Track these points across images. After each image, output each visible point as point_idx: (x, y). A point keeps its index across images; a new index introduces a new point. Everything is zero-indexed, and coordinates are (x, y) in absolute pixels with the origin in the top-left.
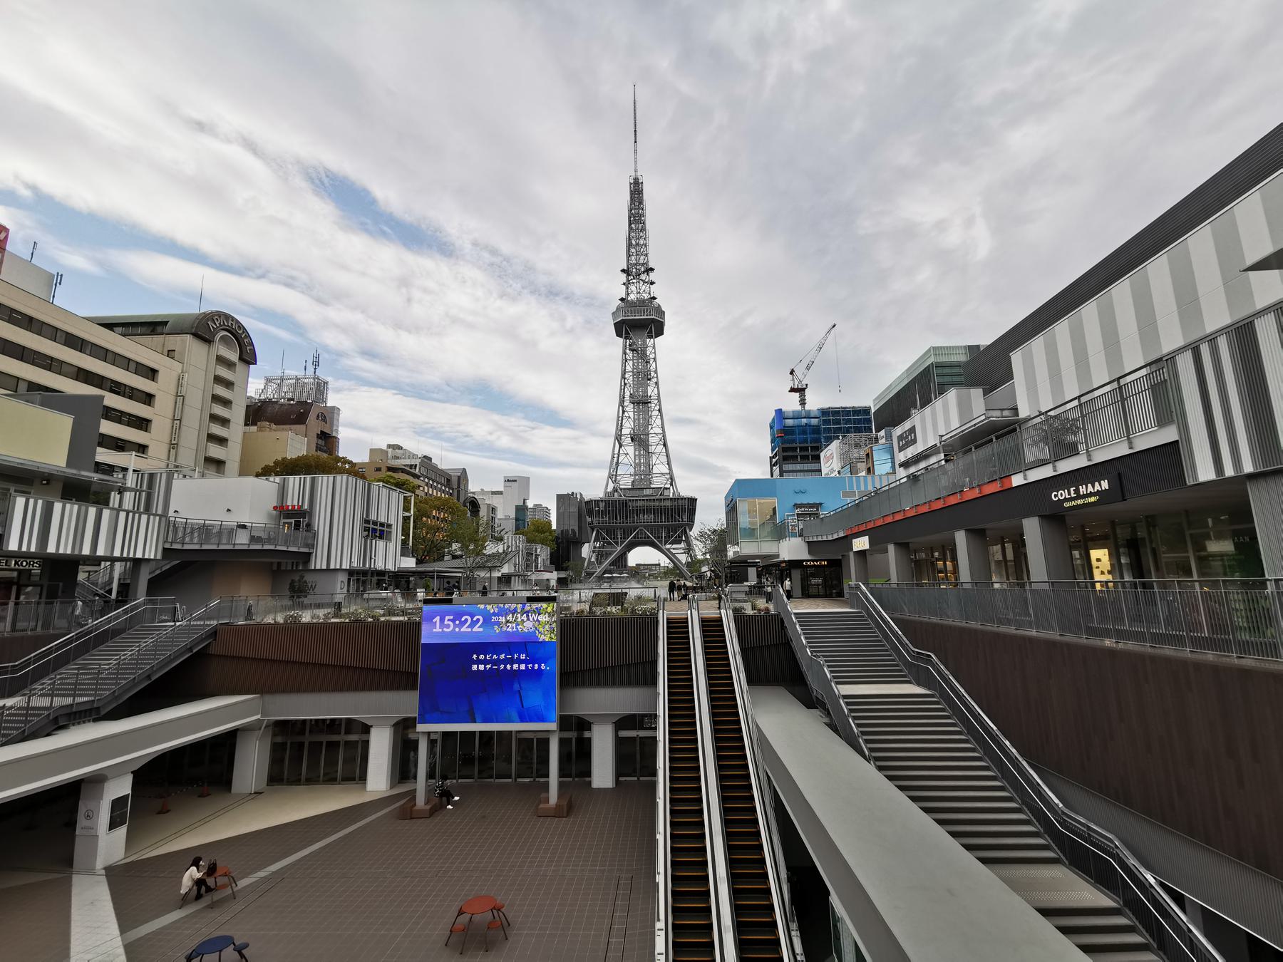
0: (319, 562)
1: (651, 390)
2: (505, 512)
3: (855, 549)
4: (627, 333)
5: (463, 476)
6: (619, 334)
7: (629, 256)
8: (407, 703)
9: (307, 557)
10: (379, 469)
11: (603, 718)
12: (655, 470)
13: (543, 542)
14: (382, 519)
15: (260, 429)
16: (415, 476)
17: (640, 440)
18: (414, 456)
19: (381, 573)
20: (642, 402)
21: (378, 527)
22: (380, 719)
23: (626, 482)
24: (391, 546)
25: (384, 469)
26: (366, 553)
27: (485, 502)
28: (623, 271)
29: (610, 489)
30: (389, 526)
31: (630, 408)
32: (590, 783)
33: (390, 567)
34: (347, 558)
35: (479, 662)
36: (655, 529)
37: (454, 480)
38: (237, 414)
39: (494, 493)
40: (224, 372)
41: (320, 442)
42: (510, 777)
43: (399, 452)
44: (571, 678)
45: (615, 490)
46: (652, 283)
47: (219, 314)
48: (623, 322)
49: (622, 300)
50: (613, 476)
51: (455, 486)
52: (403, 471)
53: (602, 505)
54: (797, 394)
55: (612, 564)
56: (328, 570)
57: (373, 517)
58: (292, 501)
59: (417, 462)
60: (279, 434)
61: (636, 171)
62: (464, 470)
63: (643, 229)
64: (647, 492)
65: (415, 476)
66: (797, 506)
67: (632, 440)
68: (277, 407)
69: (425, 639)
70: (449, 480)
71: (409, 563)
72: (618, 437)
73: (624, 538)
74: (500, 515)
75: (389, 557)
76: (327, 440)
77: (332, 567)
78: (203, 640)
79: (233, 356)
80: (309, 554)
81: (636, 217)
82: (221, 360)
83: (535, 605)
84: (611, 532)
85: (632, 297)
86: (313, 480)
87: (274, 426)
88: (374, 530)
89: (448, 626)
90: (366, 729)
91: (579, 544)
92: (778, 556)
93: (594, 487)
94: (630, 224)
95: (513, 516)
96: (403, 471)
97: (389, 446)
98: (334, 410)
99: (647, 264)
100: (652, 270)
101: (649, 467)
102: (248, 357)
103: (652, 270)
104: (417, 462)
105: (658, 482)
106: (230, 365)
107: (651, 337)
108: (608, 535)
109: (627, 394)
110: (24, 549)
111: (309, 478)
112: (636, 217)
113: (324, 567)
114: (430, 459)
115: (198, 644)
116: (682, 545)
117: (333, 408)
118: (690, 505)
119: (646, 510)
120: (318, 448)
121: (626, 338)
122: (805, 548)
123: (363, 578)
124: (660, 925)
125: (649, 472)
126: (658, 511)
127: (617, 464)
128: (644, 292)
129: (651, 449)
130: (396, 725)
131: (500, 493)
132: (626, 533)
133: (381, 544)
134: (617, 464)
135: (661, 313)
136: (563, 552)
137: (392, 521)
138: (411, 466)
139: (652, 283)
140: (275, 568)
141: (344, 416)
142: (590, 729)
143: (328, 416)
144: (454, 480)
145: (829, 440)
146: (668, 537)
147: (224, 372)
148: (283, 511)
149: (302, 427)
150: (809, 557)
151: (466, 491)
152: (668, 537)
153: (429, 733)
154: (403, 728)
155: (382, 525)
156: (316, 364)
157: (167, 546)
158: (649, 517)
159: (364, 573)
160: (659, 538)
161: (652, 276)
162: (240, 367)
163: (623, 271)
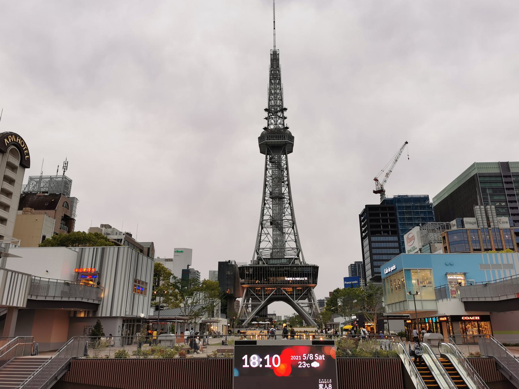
0: (104, 312)
1: (285, 190)
6: (262, 152)
12: (287, 246)
14: (143, 279)
15: (24, 213)
17: (276, 224)
20: (278, 198)
23: (266, 254)
24: (146, 298)
30: (147, 283)
31: (270, 203)
34: (121, 310)
37: (146, 250)
38: (14, 202)
39: (167, 260)
40: (10, 173)
41: (63, 222)
43: (109, 231)
45: (259, 259)
47: (12, 134)
50: (258, 250)
53: (251, 270)
54: (379, 195)
55: (257, 314)
57: (139, 278)
58: (86, 267)
59: (123, 237)
60: (37, 217)
61: (275, 46)
62: (153, 243)
63: (279, 83)
64: (283, 261)
68: (36, 197)
76: (68, 221)
77: (114, 315)
78: (61, 372)
79: (16, 162)
80: (98, 305)
81: (275, 75)
85: (272, 127)
86: (103, 249)
87: (33, 211)
93: (244, 258)
97: (102, 226)
98: (74, 200)
99: (282, 106)
100: (286, 109)
101: (283, 242)
102: (25, 163)
103: (286, 109)
104: (123, 237)
105: (290, 254)
106: (13, 168)
110: (8, 304)
112: (275, 75)
113: (108, 315)
114: (131, 235)
115: (59, 375)
116: (306, 301)
117: (74, 198)
118: (313, 272)
123: (132, 323)
125: (283, 248)
129: (286, 230)
133: (141, 297)
137: (148, 281)
138: (118, 240)
140: (72, 315)
143: (70, 204)
144: (146, 250)
145: (413, 225)
147: (10, 173)
148: (80, 275)
149: (52, 212)
150: (465, 313)
155: (143, 283)
156: (65, 168)
157: (29, 298)
161: (286, 114)
162: (19, 169)
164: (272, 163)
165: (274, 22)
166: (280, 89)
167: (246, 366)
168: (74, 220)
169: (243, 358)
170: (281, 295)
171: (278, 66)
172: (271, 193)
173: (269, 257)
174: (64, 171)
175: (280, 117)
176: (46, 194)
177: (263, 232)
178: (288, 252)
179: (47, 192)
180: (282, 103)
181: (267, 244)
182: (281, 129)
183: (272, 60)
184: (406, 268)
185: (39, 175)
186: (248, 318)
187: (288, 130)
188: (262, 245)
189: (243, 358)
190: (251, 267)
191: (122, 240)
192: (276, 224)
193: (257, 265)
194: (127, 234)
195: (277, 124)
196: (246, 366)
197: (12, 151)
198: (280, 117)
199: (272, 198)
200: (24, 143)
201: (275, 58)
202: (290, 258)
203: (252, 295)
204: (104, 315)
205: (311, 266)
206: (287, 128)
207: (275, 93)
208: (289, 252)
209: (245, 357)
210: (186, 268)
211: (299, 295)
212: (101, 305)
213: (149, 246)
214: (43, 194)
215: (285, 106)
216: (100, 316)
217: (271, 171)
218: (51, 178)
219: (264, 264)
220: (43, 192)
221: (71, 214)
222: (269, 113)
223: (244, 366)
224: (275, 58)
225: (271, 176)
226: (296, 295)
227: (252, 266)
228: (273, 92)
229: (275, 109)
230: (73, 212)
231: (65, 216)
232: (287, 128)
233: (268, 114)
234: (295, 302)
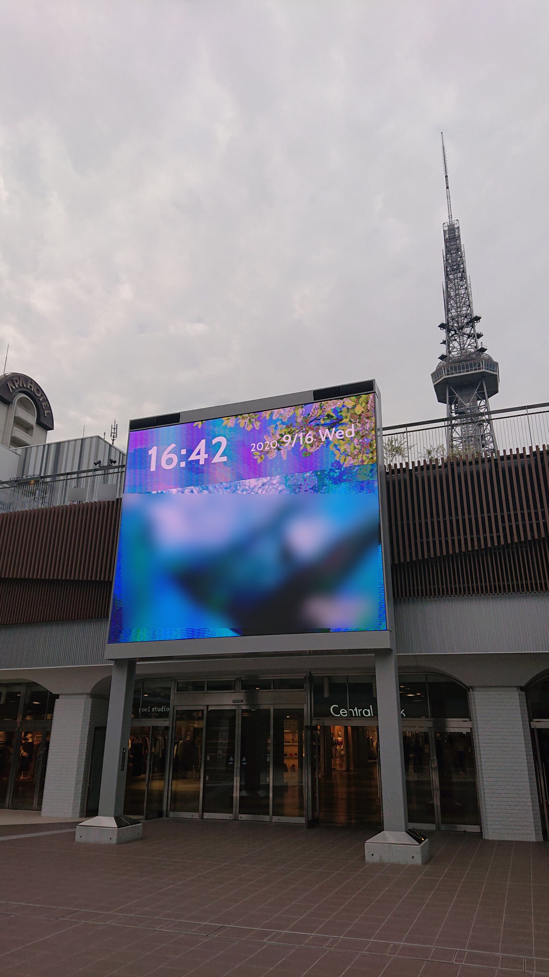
0: (285, 773)
7: (448, 311)
28: (442, 326)
35: (306, 734)
40: (20, 434)
46: (479, 336)
48: (446, 382)
49: (442, 357)
61: (450, 217)
79: (32, 420)
82: (19, 423)
83: (330, 405)
94: (447, 275)
100: (478, 319)
102: (46, 423)
103: (478, 319)
106: (28, 428)
124: (8, 796)
128: (470, 345)
135: (494, 365)
139: (479, 336)
142: (465, 713)
147: (20, 434)
161: (479, 327)
162: (37, 430)
163: (442, 326)
165: (446, 177)
166: (469, 306)
169: (225, 459)
171: (458, 249)
180: (472, 311)
182: (471, 354)
183: (448, 251)
187: (486, 352)
197: (22, 402)
198: (469, 336)
200: (39, 389)
201: (452, 238)
206: (483, 350)
215: (475, 314)
222: (449, 331)
224: (452, 238)
225: (461, 438)
228: (452, 294)
229: (459, 321)
232: (483, 350)
233: (448, 334)
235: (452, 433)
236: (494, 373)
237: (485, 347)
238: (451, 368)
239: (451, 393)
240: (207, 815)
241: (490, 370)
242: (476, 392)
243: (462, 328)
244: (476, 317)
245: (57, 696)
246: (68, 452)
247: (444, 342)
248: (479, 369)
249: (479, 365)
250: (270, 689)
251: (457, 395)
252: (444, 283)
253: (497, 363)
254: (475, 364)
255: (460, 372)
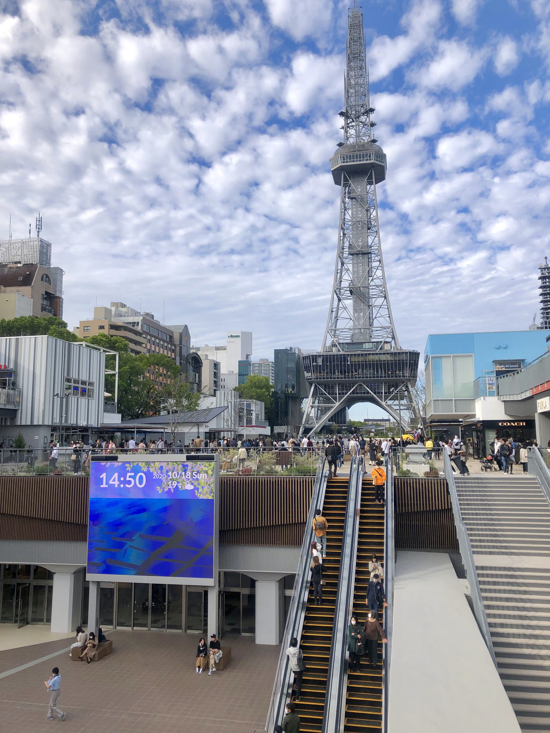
0: (24, 419)
2: (229, 366)
3: (540, 410)
4: (346, 180)
5: (185, 333)
8: (77, 553)
9: (13, 413)
10: (102, 327)
11: (268, 576)
12: (376, 323)
13: (259, 398)
16: (136, 333)
17: (360, 294)
18: (136, 314)
19: (85, 429)
21: (80, 386)
22: (63, 564)
24: (93, 403)
25: (107, 327)
26: (65, 410)
27: (208, 357)
29: (329, 344)
30: (91, 384)
32: (253, 639)
33: (93, 423)
36: (375, 386)
39: (217, 349)
41: (45, 302)
42: (179, 627)
43: (124, 310)
44: (231, 535)
45: (334, 345)
46: (373, 125)
48: (341, 168)
50: (334, 331)
51: (177, 342)
52: (126, 329)
53: (320, 361)
56: (32, 426)
57: (74, 375)
59: (139, 319)
62: (186, 326)
64: (367, 346)
65: (136, 333)
66: (496, 362)
67: (351, 292)
68: (6, 270)
69: (93, 493)
70: (171, 337)
71: (114, 419)
72: (337, 291)
73: (342, 394)
74: (223, 370)
75: (92, 412)
76: (52, 301)
77: (35, 423)
80: (16, 411)
84: (329, 387)
88: (76, 388)
89: (129, 483)
90: (49, 575)
91: (298, 399)
92: (474, 416)
93: (313, 342)
95: (236, 371)
96: (126, 329)
97: (113, 304)
104: (139, 319)
105: (378, 336)
107: (371, 183)
108: (325, 391)
109: (347, 244)
111: (13, 338)
113: (29, 423)
114: (153, 317)
116: (404, 402)
119: (366, 365)
120: (43, 309)
121: (345, 185)
122: (501, 407)
126: (378, 365)
127: (336, 317)
129: (373, 302)
130: (76, 573)
131: (224, 348)
132: (345, 387)
133: (83, 401)
134: (336, 317)
136: (281, 409)
137: (94, 379)
138: (134, 323)
139: (373, 125)
141: (67, 279)
143: (52, 277)
144: (176, 337)
146: (388, 393)
151: (188, 348)
152: (388, 393)
153: (98, 583)
154: (80, 575)
155: (84, 383)
158: (369, 372)
159: (67, 429)
160: (379, 393)
164: (352, 198)
167: (104, 485)
168: (60, 298)
169: (101, 477)
170: (364, 393)
172: (350, 247)
173: (349, 341)
174: (38, 232)
175: (364, 124)
176: (19, 265)
177: (341, 305)
178: (375, 334)
179: (20, 263)
181: (345, 324)
184: (433, 355)
185: (8, 238)
186: (317, 426)
187: (377, 143)
188: (341, 324)
189: (101, 477)
190: (320, 356)
191: (138, 323)
192: (360, 294)
193: (329, 353)
194: (147, 314)
195: (359, 136)
196: (104, 485)
199: (352, 255)
202: (377, 342)
203: (322, 394)
204: (23, 423)
205: (406, 353)
206: (374, 141)
207: (357, 84)
208: (379, 333)
209: (104, 476)
210: (245, 359)
211: (343, 394)
212: (20, 411)
213: (181, 331)
214: (16, 265)
216: (19, 424)
217: (350, 212)
218: (23, 242)
219: (339, 351)
220: (16, 263)
221: (55, 291)
223: (102, 486)
226: (339, 394)
227: (322, 354)
228: (353, 82)
230: (58, 288)
231: (47, 293)
232: (374, 141)
233: (345, 120)
234: (383, 403)
235: (345, 215)
236: (382, 164)
237: (376, 139)
238: (347, 157)
239: (345, 176)
240: (135, 628)
241: (379, 161)
242: (366, 181)
243: (358, 117)
244: (371, 109)
245: (55, 573)
246: (24, 358)
247: (343, 128)
248: (370, 160)
249: (370, 156)
250: (106, 367)
251: (350, 182)
252: (346, 71)
253: (385, 155)
254: (367, 155)
255: (354, 161)
